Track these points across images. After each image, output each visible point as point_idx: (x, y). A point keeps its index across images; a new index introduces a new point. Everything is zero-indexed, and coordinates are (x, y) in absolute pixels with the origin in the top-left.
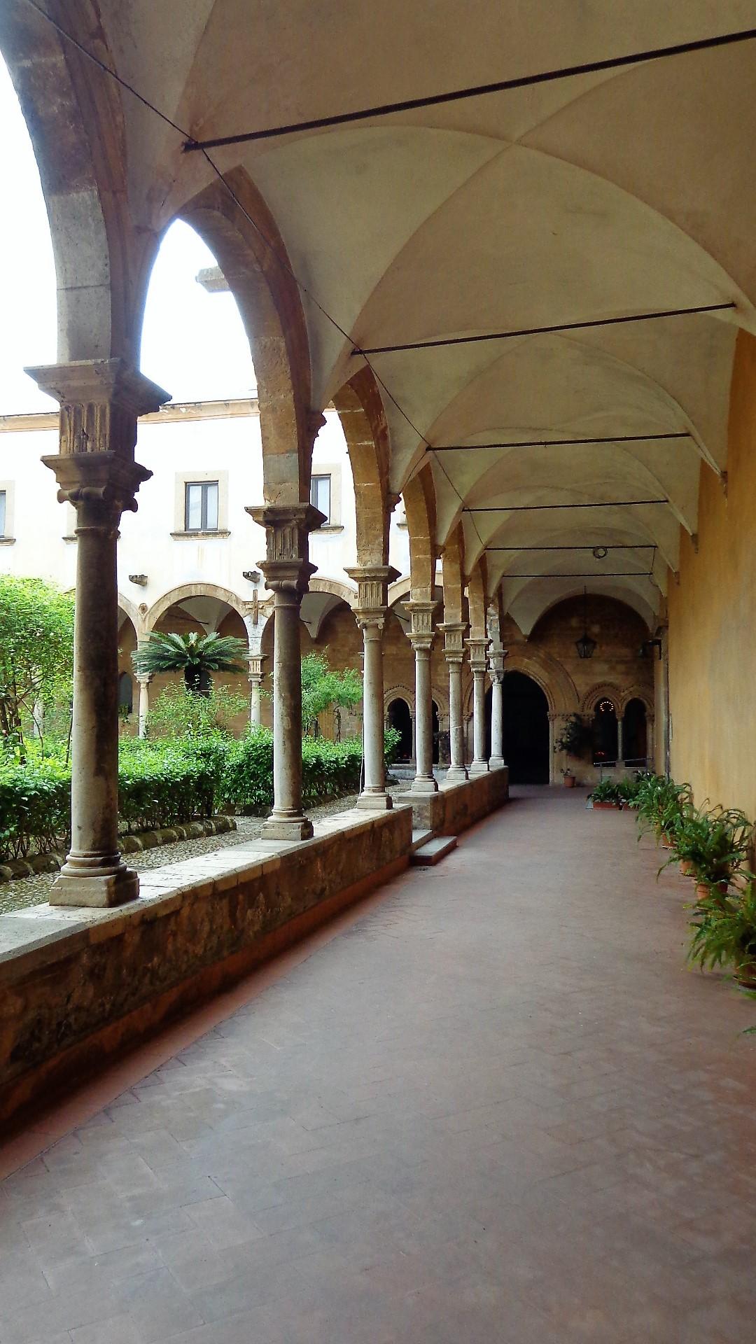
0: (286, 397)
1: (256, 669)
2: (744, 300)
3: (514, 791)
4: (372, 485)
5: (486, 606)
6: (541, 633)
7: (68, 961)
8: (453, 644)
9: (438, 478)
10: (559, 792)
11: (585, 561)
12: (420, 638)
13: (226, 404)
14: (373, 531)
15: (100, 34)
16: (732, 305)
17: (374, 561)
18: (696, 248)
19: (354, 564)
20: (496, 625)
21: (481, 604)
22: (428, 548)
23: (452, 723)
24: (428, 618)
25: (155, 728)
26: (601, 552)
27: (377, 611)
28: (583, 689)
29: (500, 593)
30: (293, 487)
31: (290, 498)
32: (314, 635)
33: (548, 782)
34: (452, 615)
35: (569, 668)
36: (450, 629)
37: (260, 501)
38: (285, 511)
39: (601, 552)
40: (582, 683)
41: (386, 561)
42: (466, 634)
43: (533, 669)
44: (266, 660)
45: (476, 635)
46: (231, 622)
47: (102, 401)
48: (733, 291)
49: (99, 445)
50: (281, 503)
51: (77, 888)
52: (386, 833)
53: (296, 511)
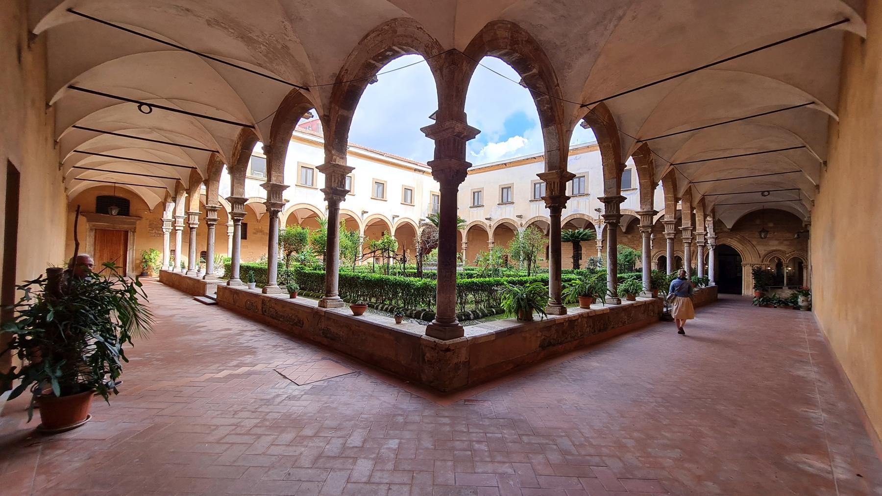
0: (612, 161)
1: (599, 244)
2: (817, 101)
3: (720, 296)
4: (647, 181)
5: (705, 218)
6: (739, 226)
7: (551, 326)
8: (686, 235)
9: (677, 175)
10: (748, 301)
11: (758, 197)
12: (669, 234)
13: (505, 164)
14: (647, 196)
15: (558, 85)
16: (813, 103)
17: (647, 208)
18: (790, 86)
19: (639, 210)
20: (711, 225)
21: (702, 218)
22: (673, 196)
23: (699, 264)
24: (673, 226)
25: (603, 280)
26: (766, 193)
27: (648, 226)
28: (762, 253)
29: (713, 211)
30: (614, 190)
31: (613, 194)
32: (624, 230)
33: (741, 293)
34: (686, 223)
35: (754, 243)
36: (685, 229)
37: (602, 195)
38: (612, 198)
39: (766, 193)
40: (762, 250)
41: (652, 208)
42: (694, 229)
43: (734, 243)
44: (604, 241)
45: (700, 229)
46: (590, 226)
47: (557, 181)
48: (811, 98)
49: (556, 192)
50: (610, 195)
51: (551, 310)
52: (651, 307)
53: (615, 198)
